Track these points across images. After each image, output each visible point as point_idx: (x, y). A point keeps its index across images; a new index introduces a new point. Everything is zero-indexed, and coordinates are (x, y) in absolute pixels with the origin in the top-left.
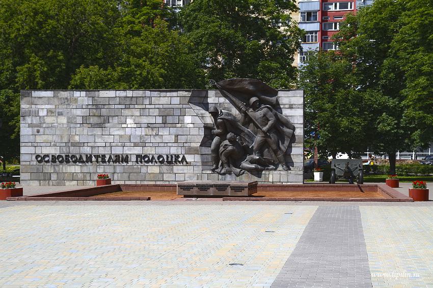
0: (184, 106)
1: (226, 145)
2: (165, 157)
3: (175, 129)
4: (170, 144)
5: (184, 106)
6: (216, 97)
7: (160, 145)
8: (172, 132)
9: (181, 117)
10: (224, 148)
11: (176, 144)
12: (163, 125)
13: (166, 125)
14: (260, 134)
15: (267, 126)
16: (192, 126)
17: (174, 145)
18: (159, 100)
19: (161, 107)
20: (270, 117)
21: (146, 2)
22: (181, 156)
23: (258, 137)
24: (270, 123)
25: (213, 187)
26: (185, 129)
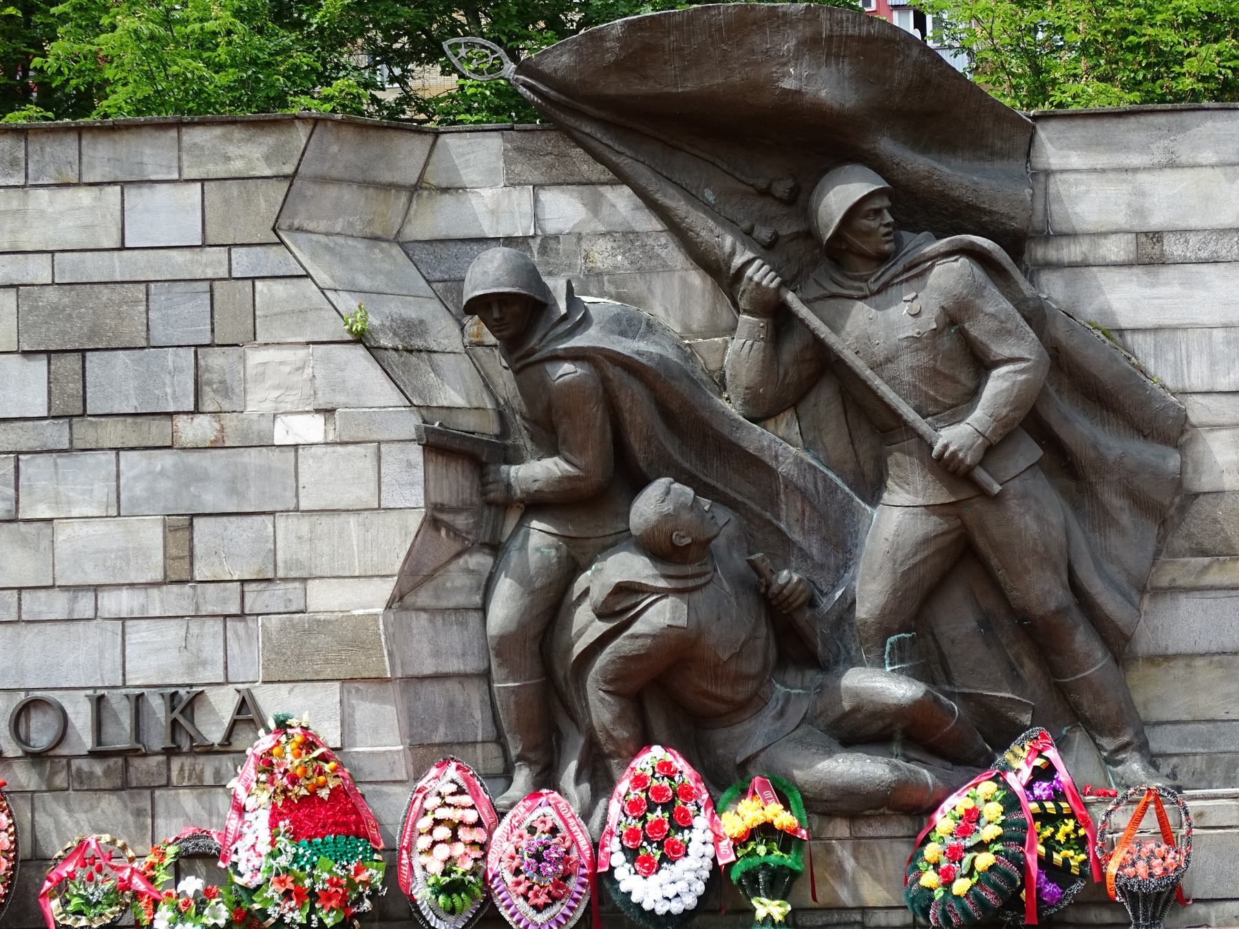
0: (243, 261)
1: (625, 590)
2: (81, 716)
3: (165, 460)
4: (114, 603)
5: (243, 261)
6: (512, 184)
7: (34, 605)
8: (139, 489)
9: (216, 360)
10: (602, 615)
11: (175, 599)
12: (57, 434)
13: (81, 428)
14: (904, 482)
15: (980, 416)
16: (311, 429)
17: (158, 601)
18: (21, 213)
19: (38, 270)
20: (1004, 333)
21: (207, 9)
22: (223, 704)
23: (896, 514)
24: (998, 384)
25: (493, 567)
26: (252, 458)
